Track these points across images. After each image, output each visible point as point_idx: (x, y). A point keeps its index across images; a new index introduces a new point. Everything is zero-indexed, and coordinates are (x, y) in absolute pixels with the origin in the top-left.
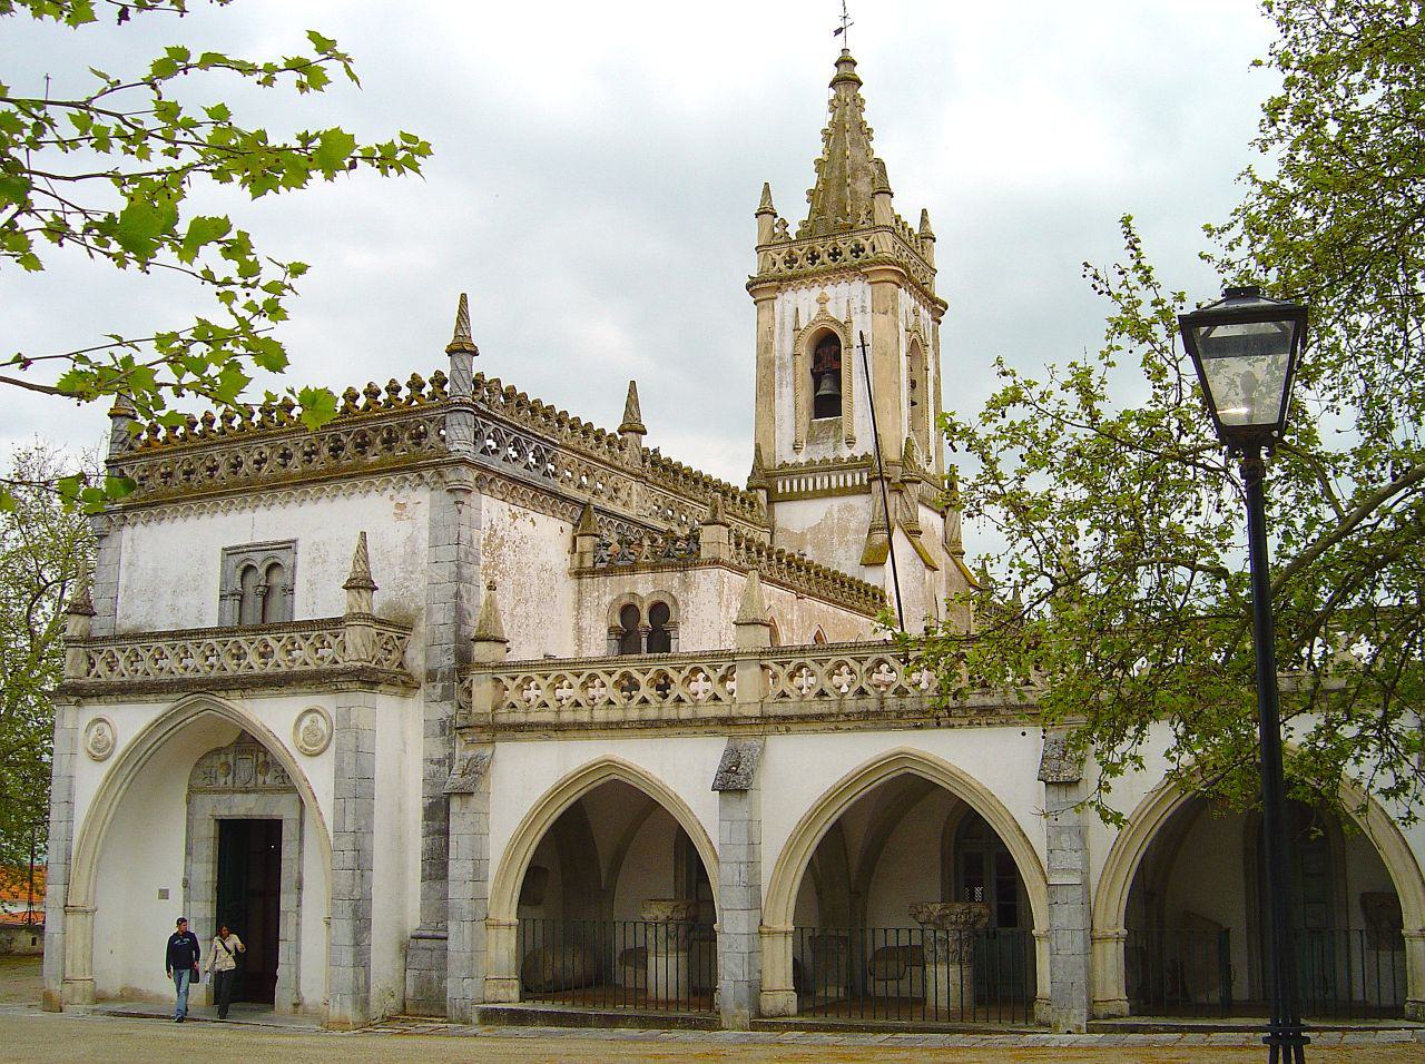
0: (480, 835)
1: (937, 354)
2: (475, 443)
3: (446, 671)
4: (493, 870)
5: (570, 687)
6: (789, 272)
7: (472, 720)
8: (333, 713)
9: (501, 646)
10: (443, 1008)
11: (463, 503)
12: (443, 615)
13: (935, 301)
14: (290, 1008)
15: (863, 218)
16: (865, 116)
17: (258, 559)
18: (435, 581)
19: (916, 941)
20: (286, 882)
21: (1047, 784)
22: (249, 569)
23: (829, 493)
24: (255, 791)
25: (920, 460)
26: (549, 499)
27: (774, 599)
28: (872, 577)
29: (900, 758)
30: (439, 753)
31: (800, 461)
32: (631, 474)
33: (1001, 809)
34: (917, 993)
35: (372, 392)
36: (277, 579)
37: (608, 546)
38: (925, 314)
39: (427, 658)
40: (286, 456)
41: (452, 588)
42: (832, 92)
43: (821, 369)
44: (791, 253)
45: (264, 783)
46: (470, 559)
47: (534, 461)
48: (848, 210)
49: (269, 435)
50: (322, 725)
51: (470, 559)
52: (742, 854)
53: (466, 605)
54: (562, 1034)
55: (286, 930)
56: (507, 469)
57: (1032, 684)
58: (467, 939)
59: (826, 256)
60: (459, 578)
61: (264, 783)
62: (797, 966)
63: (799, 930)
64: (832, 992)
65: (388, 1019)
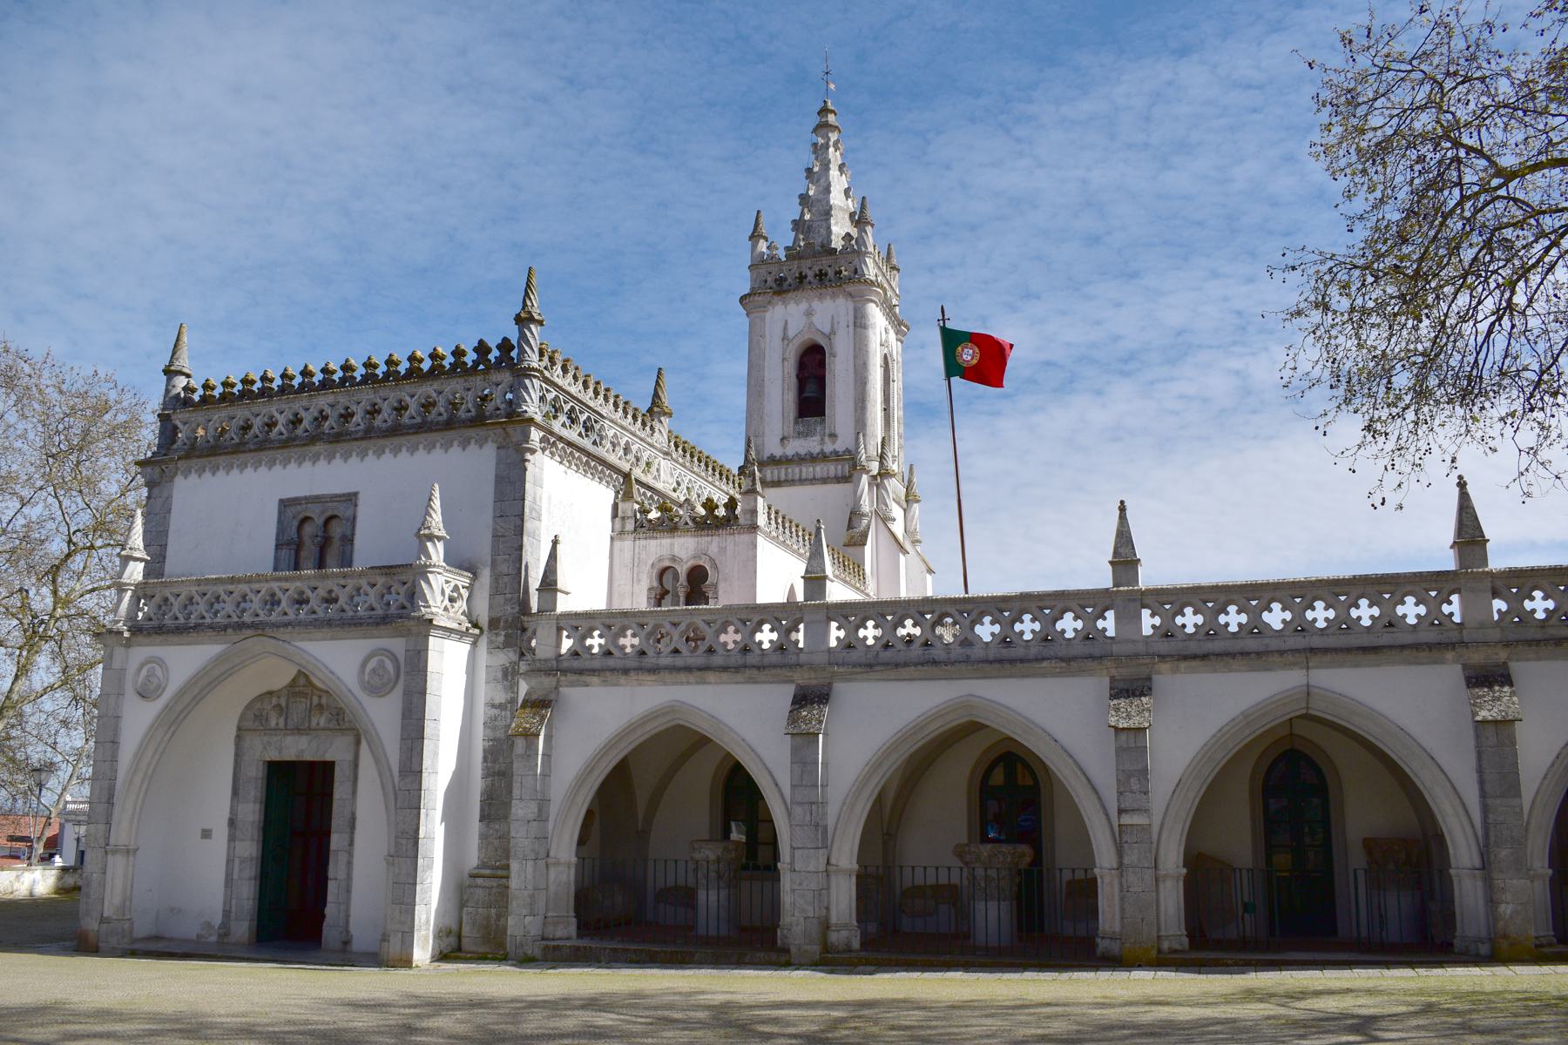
4: (554, 809)
20: (338, 821)
22: (306, 519)
23: (813, 481)
26: (594, 464)
30: (501, 697)
32: (660, 451)
33: (1195, 763)
35: (246, 381)
46: (534, 514)
55: (335, 870)
58: (529, 877)
61: (318, 724)
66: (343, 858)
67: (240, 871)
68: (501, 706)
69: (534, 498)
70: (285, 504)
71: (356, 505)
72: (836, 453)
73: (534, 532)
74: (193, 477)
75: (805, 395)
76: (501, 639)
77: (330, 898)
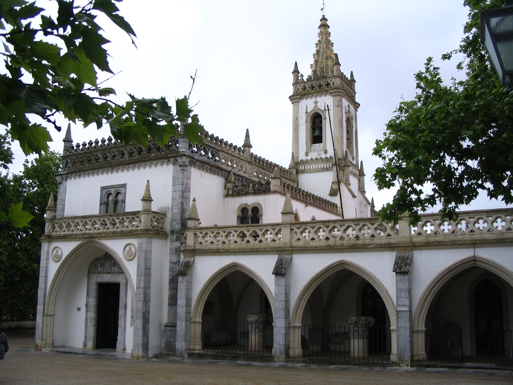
0: (189, 289)
1: (356, 122)
2: (189, 149)
3: (178, 230)
5: (222, 236)
6: (304, 93)
7: (187, 248)
8: (137, 245)
9: (198, 221)
10: (175, 351)
11: (184, 170)
12: (177, 211)
13: (356, 103)
14: (122, 351)
15: (330, 73)
16: (330, 38)
17: (113, 191)
18: (174, 198)
19: (347, 331)
21: (396, 273)
22: (110, 194)
24: (111, 273)
25: (350, 158)
27: (297, 206)
28: (336, 200)
29: (342, 263)
30: (175, 260)
31: (308, 159)
32: (247, 162)
34: (347, 350)
36: (120, 197)
37: (237, 187)
38: (352, 108)
39: (171, 226)
40: (123, 154)
41: (180, 200)
42: (319, 30)
43: (315, 127)
44: (304, 86)
45: (114, 270)
46: (187, 190)
47: (211, 156)
48: (324, 71)
49: (118, 147)
50: (133, 249)
51: (187, 190)
52: (283, 298)
53: (185, 207)
54: (215, 362)
56: (201, 158)
57: (391, 236)
59: (317, 87)
60: (183, 197)
61: (114, 270)
62: (303, 338)
63: (304, 326)
64: (315, 348)
65: (156, 356)
66: (123, 319)
67: (90, 323)
68: (175, 263)
69: (187, 184)
70: (103, 188)
71: (126, 188)
72: (312, 159)
73: (187, 197)
74: (73, 179)
75: (315, 135)
76: (175, 237)
77: (119, 333)
